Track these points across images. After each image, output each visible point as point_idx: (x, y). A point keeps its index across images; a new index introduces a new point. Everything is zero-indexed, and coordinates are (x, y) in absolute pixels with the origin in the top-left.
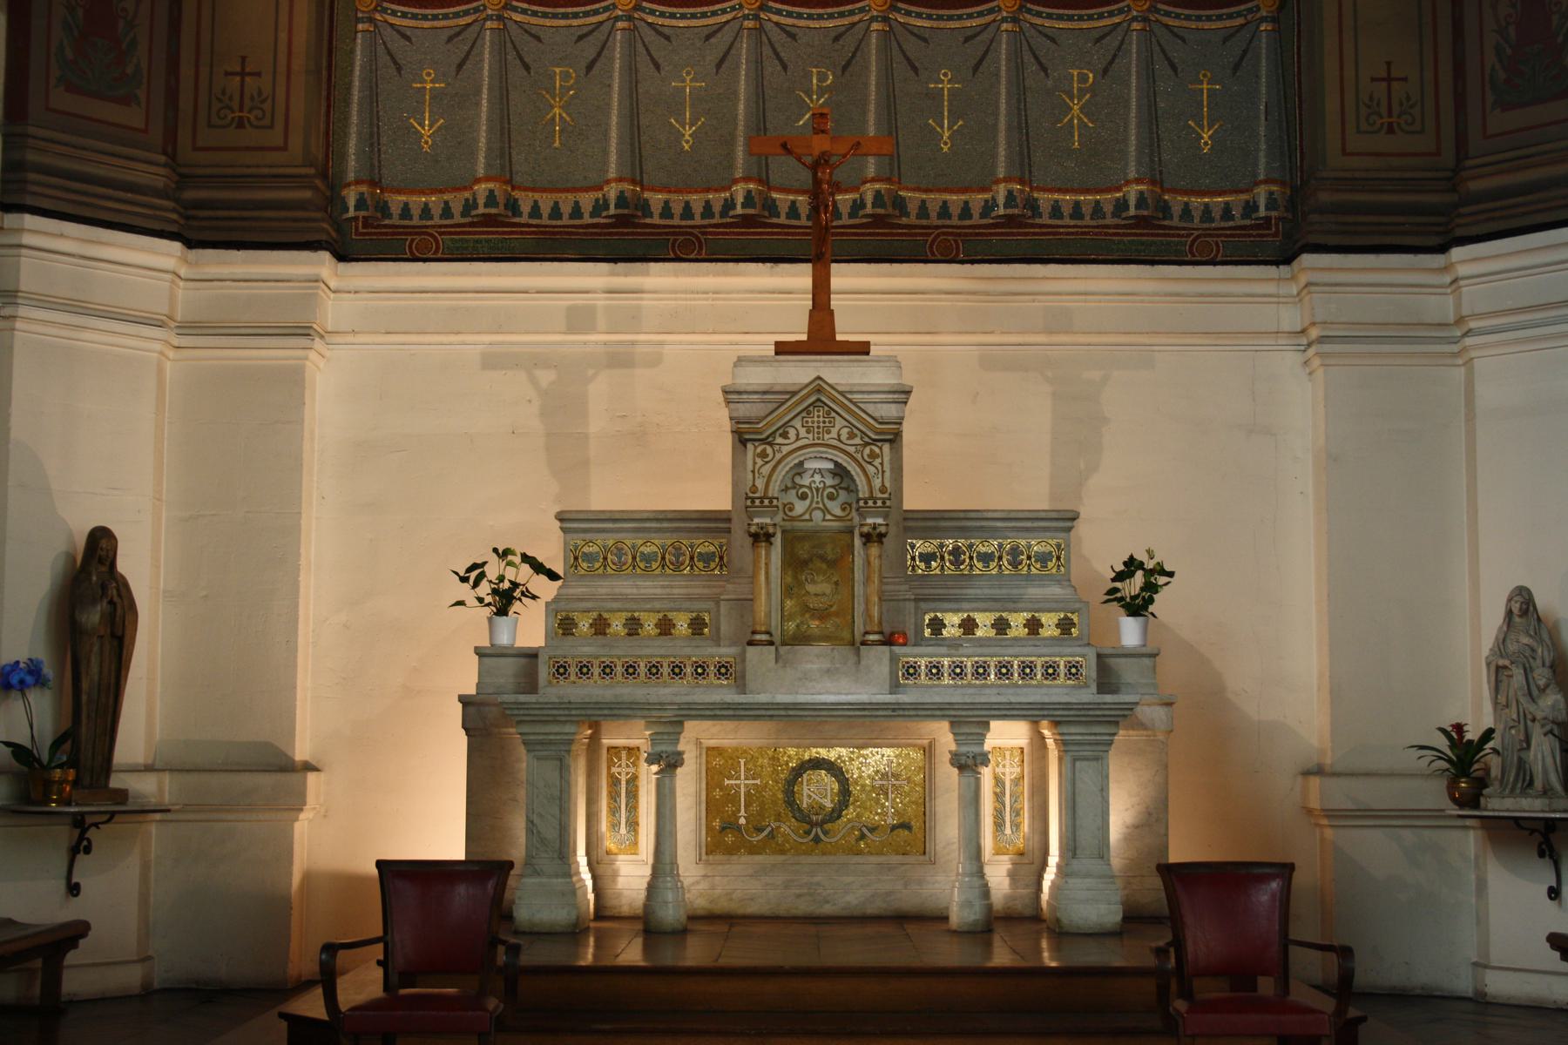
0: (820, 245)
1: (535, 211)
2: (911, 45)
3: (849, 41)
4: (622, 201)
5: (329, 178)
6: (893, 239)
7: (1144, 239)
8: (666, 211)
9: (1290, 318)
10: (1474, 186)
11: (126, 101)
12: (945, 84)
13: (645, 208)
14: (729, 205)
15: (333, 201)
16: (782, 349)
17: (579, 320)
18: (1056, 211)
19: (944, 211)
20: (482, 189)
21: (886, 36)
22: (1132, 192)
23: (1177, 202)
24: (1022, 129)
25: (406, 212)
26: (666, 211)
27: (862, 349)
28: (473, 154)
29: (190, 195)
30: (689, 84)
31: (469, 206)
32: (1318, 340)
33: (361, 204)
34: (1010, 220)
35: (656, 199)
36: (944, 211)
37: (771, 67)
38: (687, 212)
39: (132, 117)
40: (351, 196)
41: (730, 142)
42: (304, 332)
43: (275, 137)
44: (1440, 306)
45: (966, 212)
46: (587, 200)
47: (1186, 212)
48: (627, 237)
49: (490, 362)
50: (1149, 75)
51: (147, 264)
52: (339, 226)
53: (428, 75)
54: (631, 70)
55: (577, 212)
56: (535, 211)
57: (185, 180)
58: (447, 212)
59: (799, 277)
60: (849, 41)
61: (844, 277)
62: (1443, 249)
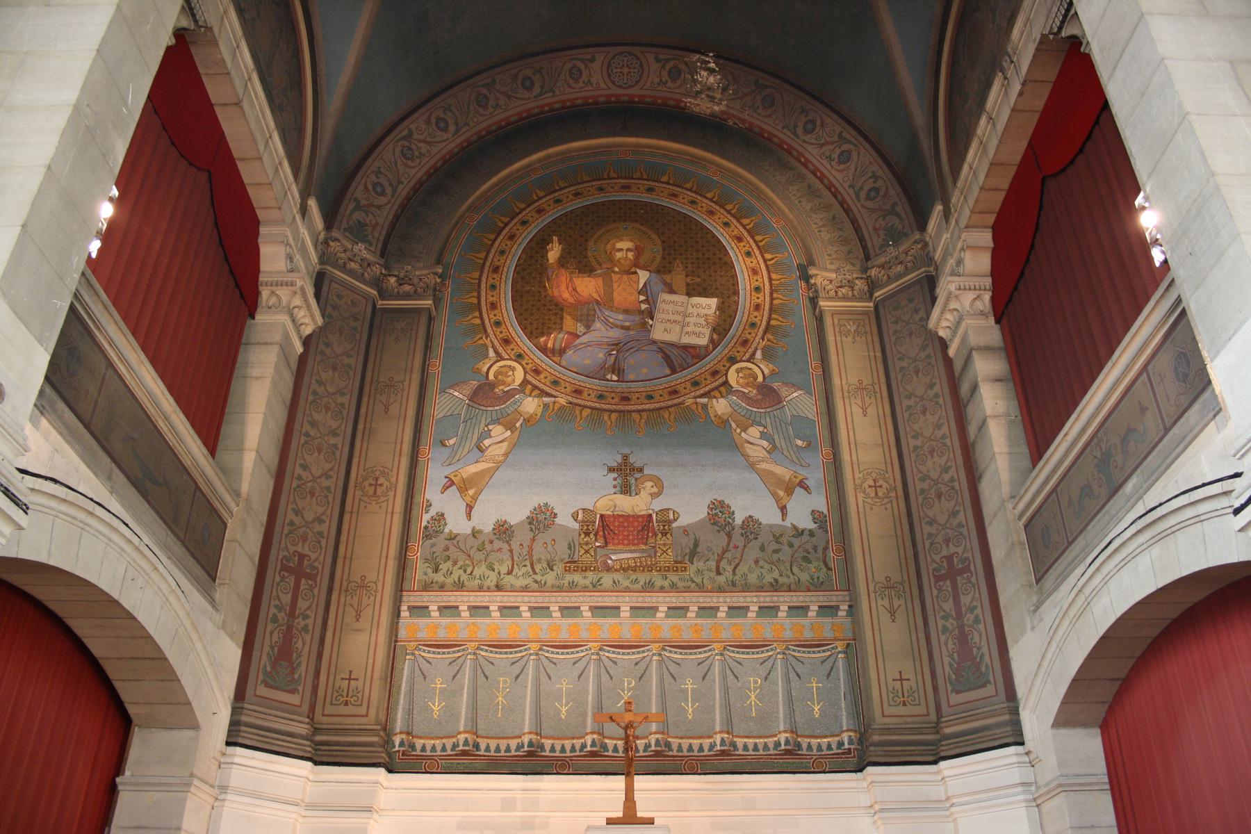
0: (629, 766)
1: (488, 749)
2: (672, 667)
3: (643, 665)
4: (531, 744)
5: (386, 730)
6: (666, 763)
7: (790, 761)
8: (553, 749)
9: (865, 799)
10: (947, 731)
11: (292, 692)
12: (689, 685)
13: (542, 748)
14: (584, 746)
15: (388, 742)
16: (610, 821)
17: (508, 805)
18: (745, 748)
19: (690, 748)
20: (462, 737)
21: (661, 662)
22: (782, 737)
23: (804, 742)
24: (727, 705)
25: (424, 748)
26: (553, 749)
27: (650, 821)
28: (458, 720)
29: (319, 738)
30: (564, 686)
31: (455, 746)
32: (879, 810)
33: (402, 744)
34: (723, 753)
35: (548, 743)
36: (690, 748)
37: (605, 677)
38: (563, 749)
39: (295, 699)
40: (397, 740)
41: (584, 715)
42: (369, 810)
43: (363, 710)
44: (938, 792)
45: (701, 749)
46: (513, 744)
47: (809, 747)
48: (533, 762)
49: (461, 826)
50: (788, 680)
51: (295, 774)
52: (390, 755)
53: (439, 680)
54: (537, 680)
55: (508, 749)
56: (488, 749)
57: (317, 731)
58: (444, 749)
59: (619, 782)
60: (643, 665)
61: (640, 782)
62: (935, 762)
